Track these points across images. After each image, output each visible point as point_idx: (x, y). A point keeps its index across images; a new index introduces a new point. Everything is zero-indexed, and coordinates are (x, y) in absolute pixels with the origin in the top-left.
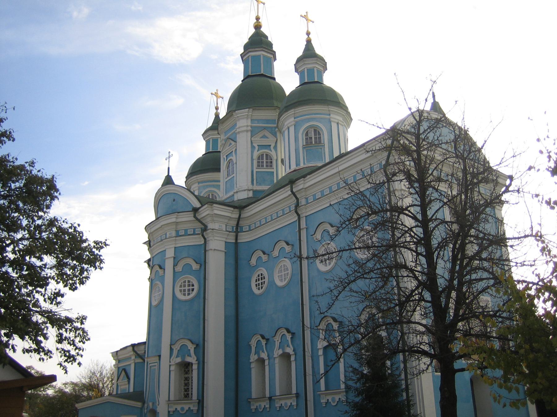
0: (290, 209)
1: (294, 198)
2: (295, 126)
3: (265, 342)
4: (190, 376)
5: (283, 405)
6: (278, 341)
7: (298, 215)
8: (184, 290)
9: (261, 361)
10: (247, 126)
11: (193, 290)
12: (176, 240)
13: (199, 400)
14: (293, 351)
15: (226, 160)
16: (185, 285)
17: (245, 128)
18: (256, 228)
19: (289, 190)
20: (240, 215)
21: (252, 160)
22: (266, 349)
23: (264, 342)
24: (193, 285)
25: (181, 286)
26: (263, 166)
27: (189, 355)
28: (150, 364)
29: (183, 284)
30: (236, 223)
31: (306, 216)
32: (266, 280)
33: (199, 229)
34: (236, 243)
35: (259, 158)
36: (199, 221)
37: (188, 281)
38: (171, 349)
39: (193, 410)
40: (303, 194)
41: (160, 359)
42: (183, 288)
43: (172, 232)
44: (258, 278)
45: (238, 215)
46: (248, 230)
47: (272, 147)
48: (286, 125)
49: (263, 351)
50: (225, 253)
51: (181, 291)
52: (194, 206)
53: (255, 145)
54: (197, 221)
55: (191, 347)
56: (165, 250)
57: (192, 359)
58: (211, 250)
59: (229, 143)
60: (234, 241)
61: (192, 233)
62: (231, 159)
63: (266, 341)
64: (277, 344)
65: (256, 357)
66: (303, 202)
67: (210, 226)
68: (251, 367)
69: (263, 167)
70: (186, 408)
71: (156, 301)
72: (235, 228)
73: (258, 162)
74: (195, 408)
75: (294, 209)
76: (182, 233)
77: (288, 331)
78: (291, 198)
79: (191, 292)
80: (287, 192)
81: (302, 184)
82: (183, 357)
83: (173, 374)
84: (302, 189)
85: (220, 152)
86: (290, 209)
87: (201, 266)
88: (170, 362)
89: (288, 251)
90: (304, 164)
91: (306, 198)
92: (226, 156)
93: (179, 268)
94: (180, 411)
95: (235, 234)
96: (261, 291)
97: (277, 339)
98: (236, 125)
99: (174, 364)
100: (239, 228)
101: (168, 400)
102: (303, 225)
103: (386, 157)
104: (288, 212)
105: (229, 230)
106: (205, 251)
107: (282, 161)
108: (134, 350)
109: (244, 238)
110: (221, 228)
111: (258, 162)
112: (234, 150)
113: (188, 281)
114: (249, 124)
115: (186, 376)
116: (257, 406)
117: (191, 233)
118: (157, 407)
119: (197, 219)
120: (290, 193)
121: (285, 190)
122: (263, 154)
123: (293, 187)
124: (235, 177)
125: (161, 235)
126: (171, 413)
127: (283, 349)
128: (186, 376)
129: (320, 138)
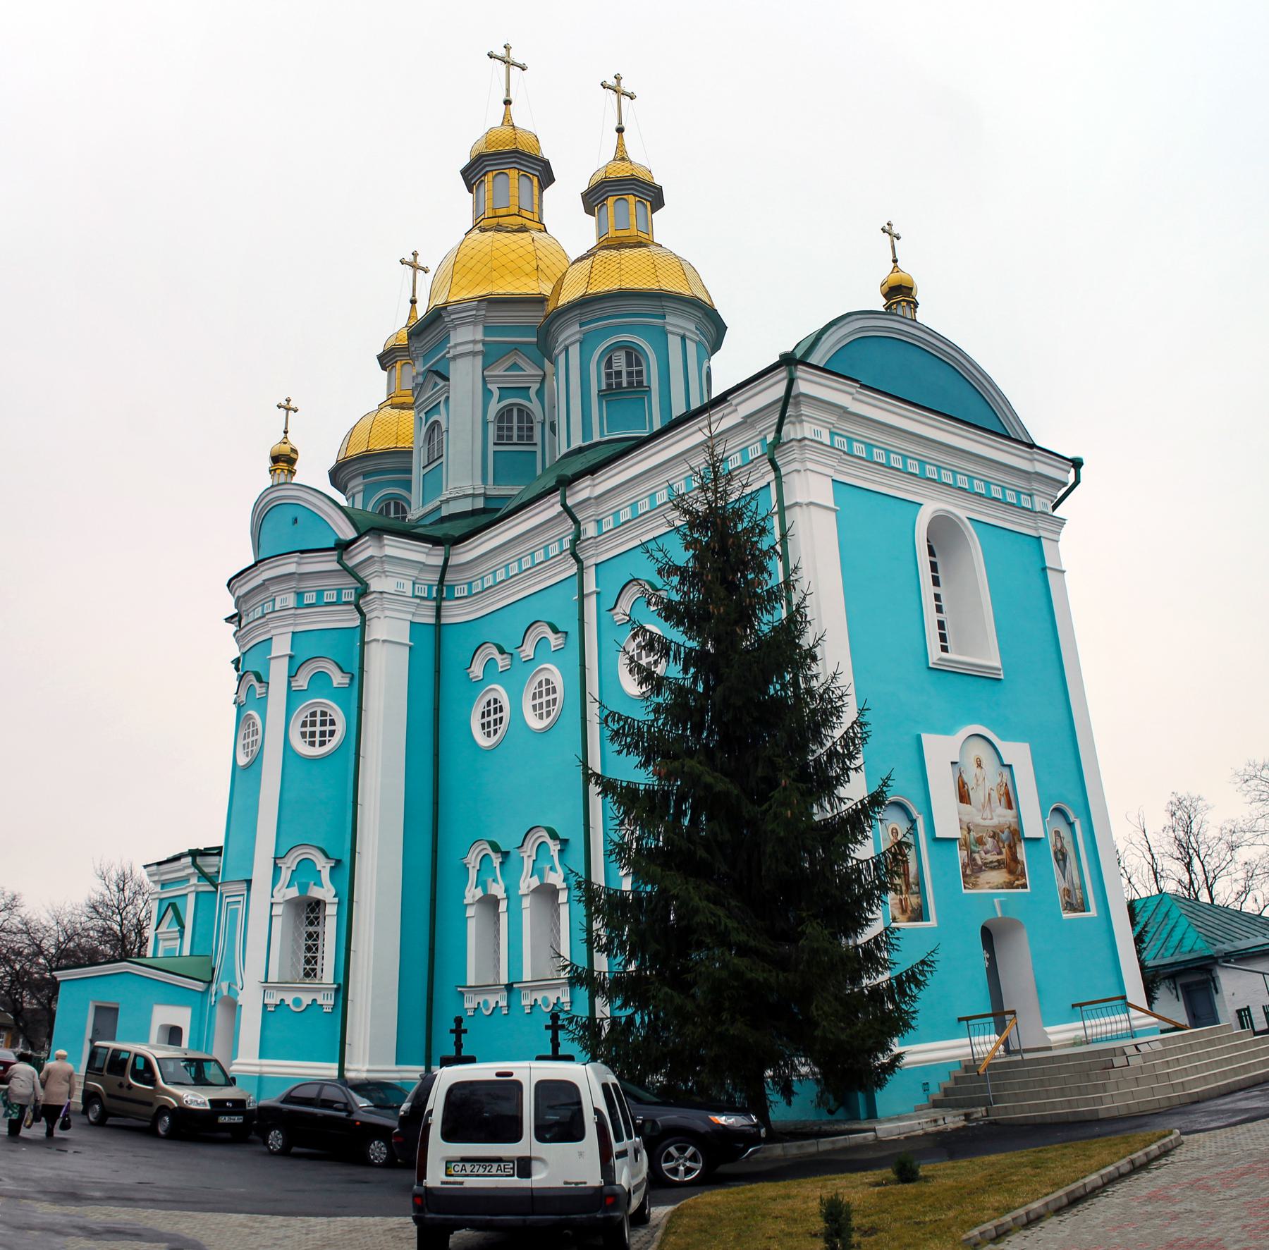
0: (561, 546)
1: (570, 522)
2: (581, 343)
3: (500, 860)
5: (539, 1002)
6: (529, 856)
7: (579, 561)
8: (313, 734)
10: (474, 342)
11: (332, 733)
12: (295, 615)
13: (339, 985)
14: (564, 880)
16: (320, 737)
17: (469, 348)
19: (557, 503)
20: (446, 560)
21: (485, 423)
23: (496, 859)
24: (332, 723)
25: (304, 724)
26: (510, 437)
27: (319, 883)
28: (226, 897)
29: (309, 719)
30: (437, 577)
31: (597, 565)
32: (506, 714)
33: (350, 591)
34: (438, 626)
37: (322, 711)
38: (277, 869)
40: (591, 511)
41: (249, 889)
42: (308, 729)
43: (287, 595)
45: (443, 558)
46: (466, 594)
47: (532, 393)
48: (561, 342)
50: (410, 648)
51: (303, 735)
52: (342, 537)
54: (346, 573)
55: (324, 866)
56: (271, 638)
57: (325, 892)
58: (377, 640)
59: (432, 384)
60: (432, 621)
61: (335, 600)
64: (528, 865)
65: (479, 893)
66: (590, 530)
67: (375, 585)
69: (512, 440)
70: (306, 999)
71: (247, 756)
72: (435, 588)
73: (500, 429)
74: (327, 1001)
76: (310, 598)
77: (553, 835)
80: (553, 505)
81: (587, 487)
82: (304, 887)
83: (277, 923)
84: (588, 499)
86: (561, 546)
87: (352, 679)
88: (272, 897)
89: (554, 647)
90: (602, 434)
92: (426, 413)
93: (302, 682)
94: (291, 1006)
95: (434, 604)
96: (494, 739)
100: (445, 588)
101: (263, 981)
102: (590, 586)
103: (775, 427)
104: (557, 553)
105: (420, 594)
106: (363, 643)
108: (194, 864)
109: (455, 614)
110: (401, 590)
112: (443, 398)
113: (322, 711)
114: (479, 336)
115: (311, 929)
117: (331, 600)
119: (345, 568)
120: (559, 508)
121: (549, 501)
122: (512, 410)
123: (567, 494)
124: (444, 464)
125: (263, 602)
126: (269, 1009)
127: (541, 877)
128: (311, 929)
129: (640, 373)
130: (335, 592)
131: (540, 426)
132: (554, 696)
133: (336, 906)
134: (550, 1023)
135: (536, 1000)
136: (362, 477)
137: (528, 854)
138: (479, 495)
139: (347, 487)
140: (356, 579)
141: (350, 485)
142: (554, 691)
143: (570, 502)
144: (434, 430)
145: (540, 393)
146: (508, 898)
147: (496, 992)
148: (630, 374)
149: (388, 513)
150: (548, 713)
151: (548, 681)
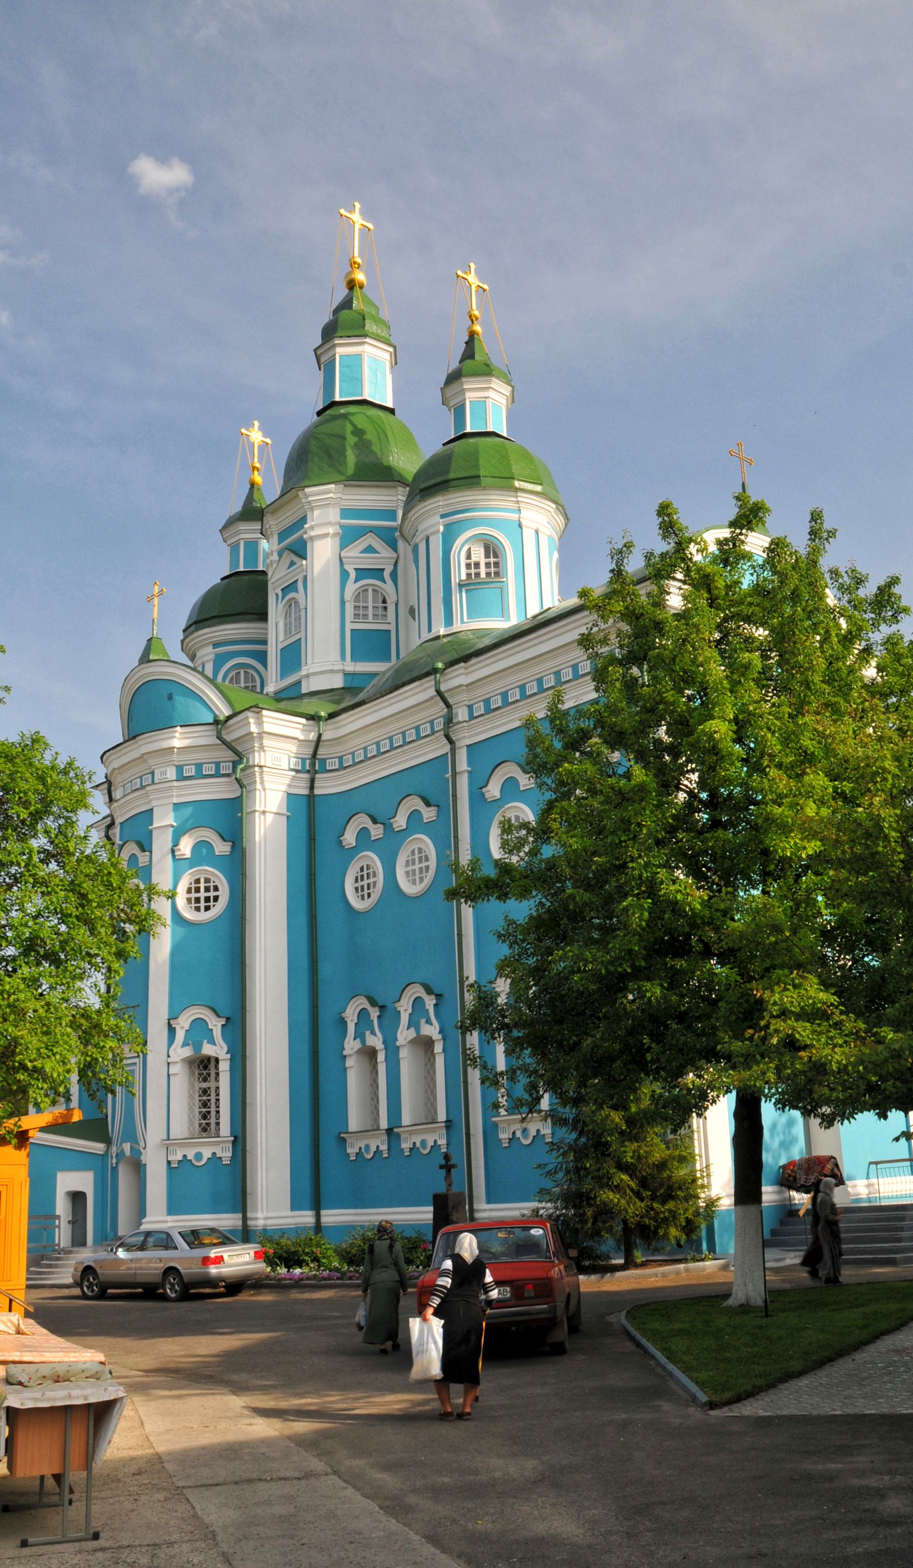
1: (442, 704)
3: (378, 1014)
4: (211, 1084)
7: (451, 741)
8: (198, 900)
9: (371, 1054)
11: (216, 899)
13: (235, 1137)
14: (440, 1033)
15: (283, 599)
18: (355, 764)
21: (343, 603)
22: (380, 1027)
23: (374, 1013)
24: (216, 889)
25: (189, 891)
26: (366, 616)
35: (357, 598)
36: (228, 745)
38: (172, 1030)
39: (220, 1158)
44: (360, 874)
46: (337, 767)
47: (387, 575)
49: (429, 1022)
50: (288, 817)
53: (350, 568)
55: (216, 1025)
57: (217, 1049)
60: (305, 792)
61: (213, 772)
62: (294, 598)
63: (380, 1011)
64: (405, 1018)
65: (412, 1034)
66: (461, 714)
68: (347, 1066)
70: (207, 1153)
72: (308, 761)
74: (226, 1154)
75: (442, 727)
77: (429, 991)
78: (436, 703)
79: (212, 903)
80: (425, 689)
85: (263, 573)
91: (469, 706)
92: (282, 590)
95: (306, 776)
97: (405, 1007)
98: (304, 520)
99: (178, 1059)
100: (317, 762)
107: (412, 611)
111: (355, 607)
112: (300, 577)
115: (205, 1085)
116: (360, 1148)
118: (141, 1154)
119: (224, 742)
122: (367, 590)
126: (173, 1166)
128: (205, 1085)
129: (496, 564)
130: (213, 765)
131: (394, 605)
132: (427, 864)
133: (228, 1062)
134: (443, 1162)
135: (414, 1143)
136: (211, 646)
137: (404, 1008)
138: (337, 671)
139: (195, 655)
140: (235, 753)
141: (199, 654)
142: (427, 859)
143: (443, 688)
144: (290, 605)
145: (394, 575)
146: (386, 1048)
147: (377, 1136)
148: (488, 565)
149: (238, 682)
150: (421, 879)
151: (420, 850)
